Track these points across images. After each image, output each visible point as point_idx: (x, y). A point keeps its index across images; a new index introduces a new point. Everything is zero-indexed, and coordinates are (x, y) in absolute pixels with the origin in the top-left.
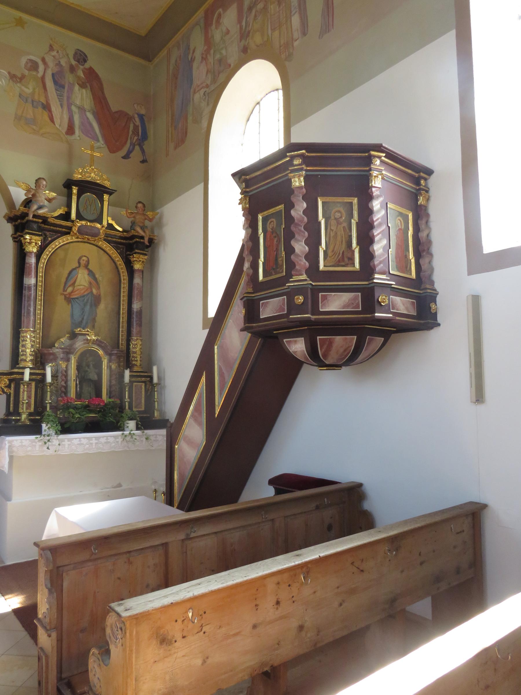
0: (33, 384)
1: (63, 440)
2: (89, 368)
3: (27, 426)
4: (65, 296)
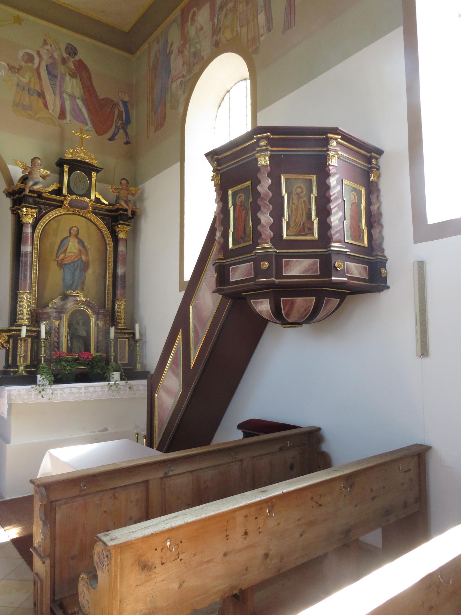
0: (30, 340)
1: (56, 390)
2: (78, 325)
3: (24, 377)
4: (57, 262)
